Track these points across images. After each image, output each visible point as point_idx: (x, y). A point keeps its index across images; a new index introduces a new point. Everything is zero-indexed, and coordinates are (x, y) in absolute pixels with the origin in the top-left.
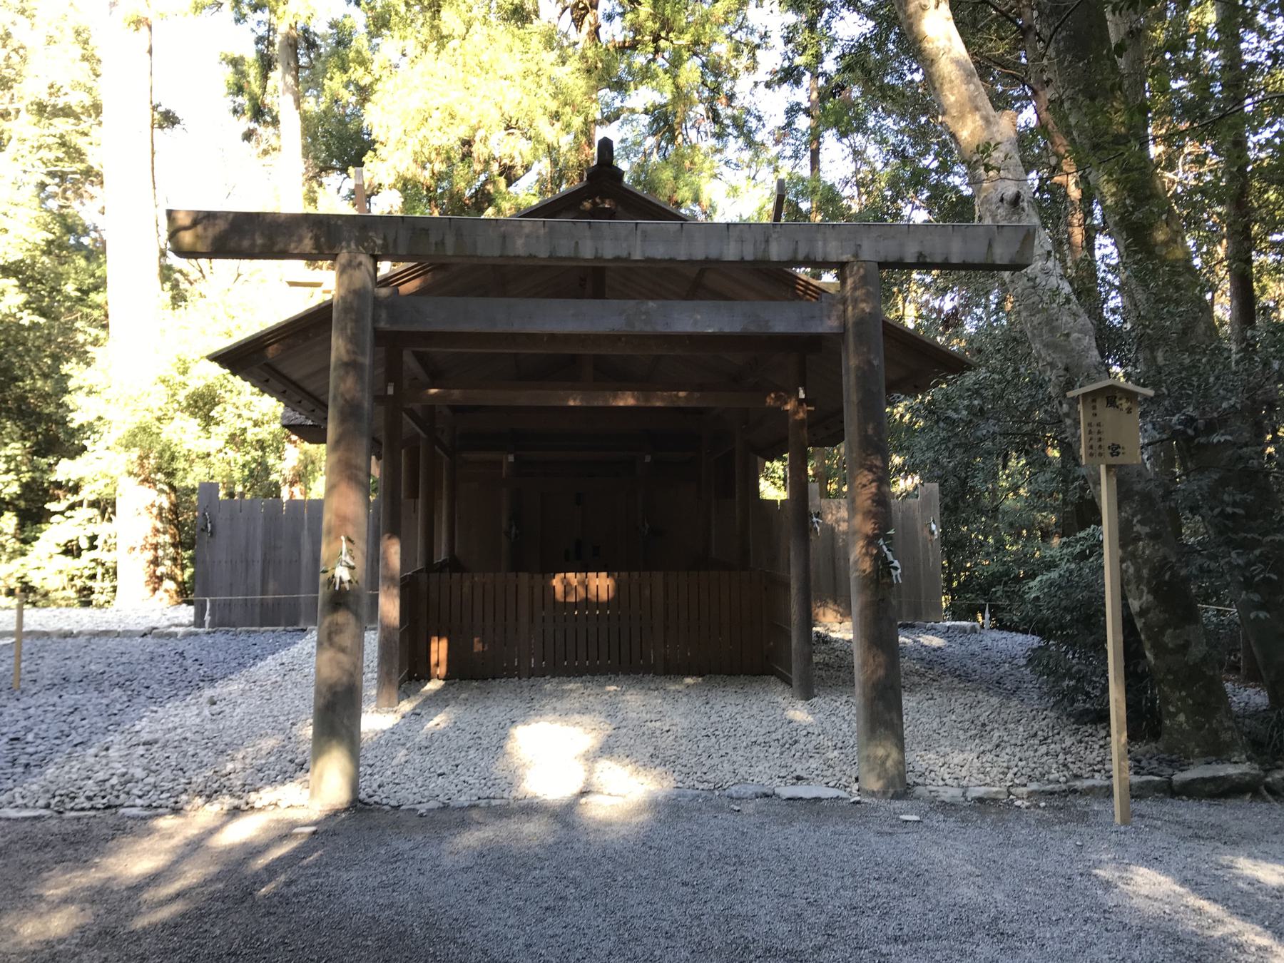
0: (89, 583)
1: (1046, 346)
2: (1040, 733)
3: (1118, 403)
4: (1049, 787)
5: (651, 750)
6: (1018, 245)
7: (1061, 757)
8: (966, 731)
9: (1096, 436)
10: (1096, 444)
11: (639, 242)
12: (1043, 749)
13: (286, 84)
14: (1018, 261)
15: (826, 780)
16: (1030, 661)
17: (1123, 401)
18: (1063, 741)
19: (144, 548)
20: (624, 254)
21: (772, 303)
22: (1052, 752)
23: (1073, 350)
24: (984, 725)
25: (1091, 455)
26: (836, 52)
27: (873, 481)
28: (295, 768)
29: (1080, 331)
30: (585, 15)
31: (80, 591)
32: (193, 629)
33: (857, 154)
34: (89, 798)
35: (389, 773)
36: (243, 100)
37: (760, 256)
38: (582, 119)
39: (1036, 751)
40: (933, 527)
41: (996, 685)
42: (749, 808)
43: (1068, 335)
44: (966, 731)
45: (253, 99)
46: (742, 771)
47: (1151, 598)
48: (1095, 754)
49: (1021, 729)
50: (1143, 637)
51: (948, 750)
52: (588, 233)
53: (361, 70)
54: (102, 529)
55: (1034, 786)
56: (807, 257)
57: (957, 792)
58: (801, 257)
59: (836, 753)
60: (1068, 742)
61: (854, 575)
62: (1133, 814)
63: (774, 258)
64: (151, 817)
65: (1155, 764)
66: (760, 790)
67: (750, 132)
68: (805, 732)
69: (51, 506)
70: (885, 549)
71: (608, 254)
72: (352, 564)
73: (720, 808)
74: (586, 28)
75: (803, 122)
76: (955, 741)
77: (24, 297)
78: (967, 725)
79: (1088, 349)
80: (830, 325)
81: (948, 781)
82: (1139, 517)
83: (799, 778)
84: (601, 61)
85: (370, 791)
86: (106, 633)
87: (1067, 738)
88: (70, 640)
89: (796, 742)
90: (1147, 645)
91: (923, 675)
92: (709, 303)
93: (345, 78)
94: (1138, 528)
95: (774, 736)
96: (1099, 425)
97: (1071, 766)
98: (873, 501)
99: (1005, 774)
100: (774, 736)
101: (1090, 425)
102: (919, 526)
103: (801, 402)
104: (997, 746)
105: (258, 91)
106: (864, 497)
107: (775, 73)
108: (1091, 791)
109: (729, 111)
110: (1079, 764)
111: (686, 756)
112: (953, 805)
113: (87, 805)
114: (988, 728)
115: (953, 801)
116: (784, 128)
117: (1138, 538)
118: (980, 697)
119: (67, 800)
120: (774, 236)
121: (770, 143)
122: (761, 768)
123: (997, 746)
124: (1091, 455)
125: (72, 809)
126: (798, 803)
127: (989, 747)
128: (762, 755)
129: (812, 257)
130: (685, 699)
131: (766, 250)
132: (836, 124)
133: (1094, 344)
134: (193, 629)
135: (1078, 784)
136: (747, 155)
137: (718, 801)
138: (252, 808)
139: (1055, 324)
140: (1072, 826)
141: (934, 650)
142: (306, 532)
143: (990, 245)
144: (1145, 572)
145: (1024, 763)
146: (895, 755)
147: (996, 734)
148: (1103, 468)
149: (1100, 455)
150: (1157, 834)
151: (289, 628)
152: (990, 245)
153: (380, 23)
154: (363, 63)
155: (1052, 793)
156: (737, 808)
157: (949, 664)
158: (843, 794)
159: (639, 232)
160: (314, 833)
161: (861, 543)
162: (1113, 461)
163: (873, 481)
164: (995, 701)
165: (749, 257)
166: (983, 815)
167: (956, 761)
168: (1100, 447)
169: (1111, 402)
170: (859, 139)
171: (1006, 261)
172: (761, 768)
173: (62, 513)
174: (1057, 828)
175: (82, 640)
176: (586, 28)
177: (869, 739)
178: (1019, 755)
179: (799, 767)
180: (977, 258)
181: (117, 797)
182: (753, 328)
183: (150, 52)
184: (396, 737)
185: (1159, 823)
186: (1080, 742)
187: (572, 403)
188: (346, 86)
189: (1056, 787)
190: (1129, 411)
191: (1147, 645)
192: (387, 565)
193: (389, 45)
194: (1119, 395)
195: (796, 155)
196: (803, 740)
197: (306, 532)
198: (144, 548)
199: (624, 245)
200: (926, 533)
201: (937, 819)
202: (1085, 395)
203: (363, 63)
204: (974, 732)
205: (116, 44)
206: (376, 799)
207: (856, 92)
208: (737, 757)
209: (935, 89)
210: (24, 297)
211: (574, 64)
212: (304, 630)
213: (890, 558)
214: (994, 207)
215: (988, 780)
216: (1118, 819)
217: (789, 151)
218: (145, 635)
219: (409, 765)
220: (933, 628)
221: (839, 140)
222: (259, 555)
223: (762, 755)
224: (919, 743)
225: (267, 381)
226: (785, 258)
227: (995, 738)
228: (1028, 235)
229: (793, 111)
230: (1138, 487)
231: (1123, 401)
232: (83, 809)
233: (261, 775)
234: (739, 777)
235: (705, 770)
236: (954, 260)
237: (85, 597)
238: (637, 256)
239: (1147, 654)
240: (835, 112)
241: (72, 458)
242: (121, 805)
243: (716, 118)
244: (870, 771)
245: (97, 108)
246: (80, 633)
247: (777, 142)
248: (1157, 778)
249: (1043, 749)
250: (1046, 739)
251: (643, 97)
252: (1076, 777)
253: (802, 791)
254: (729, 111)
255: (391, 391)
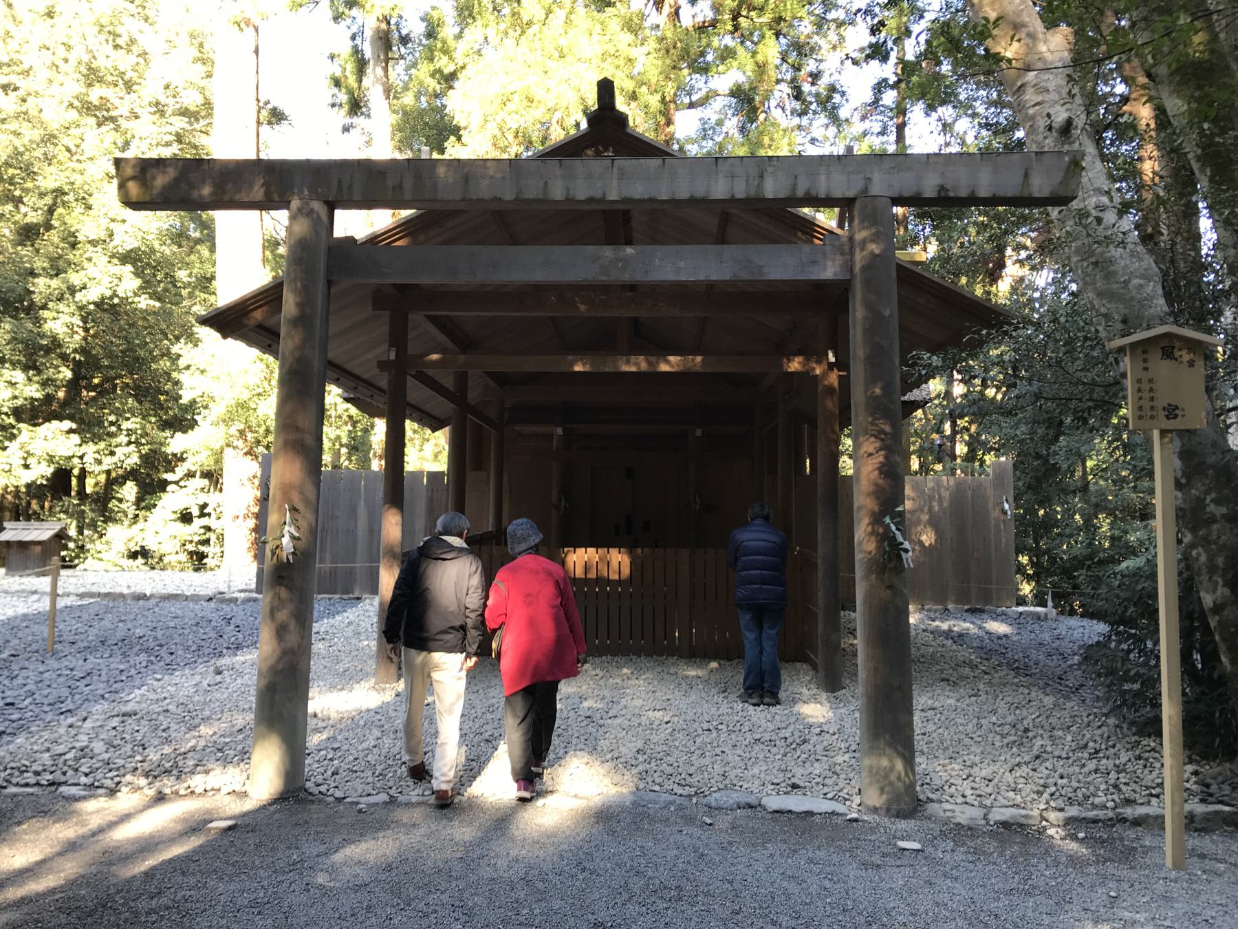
0: (202, 548)
1: (1100, 295)
2: (1091, 744)
3: (1177, 354)
4: (1091, 814)
5: (640, 744)
6: (1062, 174)
7: (1113, 775)
8: (1003, 736)
9: (1146, 395)
10: (1146, 404)
11: (615, 182)
12: (1091, 765)
14: (1062, 193)
15: (826, 790)
16: (1086, 659)
17: (1184, 353)
18: (1117, 756)
19: (246, 517)
20: (598, 195)
21: (770, 246)
22: (1102, 768)
23: (1132, 298)
24: (1026, 730)
25: (1140, 417)
26: (924, 24)
27: (881, 449)
28: (233, 753)
29: (1142, 277)
31: (191, 553)
32: (255, 595)
33: (946, 127)
34: (37, 773)
35: (351, 758)
36: (343, 97)
37: (753, 193)
38: (658, 97)
39: (1084, 765)
40: (1006, 506)
41: (1055, 682)
42: (723, 822)
43: (1126, 283)
44: (1003, 736)
45: (350, 92)
46: (732, 774)
47: (1227, 592)
48: (1154, 774)
49: (1069, 738)
50: (1217, 638)
51: (977, 759)
52: (559, 172)
53: (445, 59)
54: (213, 499)
55: (1073, 811)
56: (807, 193)
57: (977, 813)
58: (800, 193)
59: (846, 757)
60: (1124, 757)
61: (858, 557)
62: (1193, 853)
63: (769, 194)
64: (85, 798)
65: (1227, 789)
66: (743, 798)
67: (834, 108)
68: (818, 730)
69: (169, 476)
70: (893, 527)
71: (581, 194)
72: (296, 534)
73: (690, 820)
74: (666, 9)
75: (889, 97)
76: (989, 749)
77: (138, 282)
78: (1007, 729)
79: (1150, 298)
80: (830, 271)
81: (970, 799)
82: (1214, 495)
83: (795, 786)
84: (681, 41)
85: (320, 779)
86: (175, 597)
87: (1123, 753)
88: (141, 602)
89: (805, 741)
90: (1222, 648)
91: (973, 667)
92: (696, 247)
93: (432, 68)
94: (1212, 508)
95: (783, 733)
96: (1151, 381)
97: (1124, 788)
98: (881, 473)
99: (1039, 793)
100: (783, 733)
101: (1139, 381)
102: (991, 506)
103: (831, 366)
104: (1037, 757)
105: (355, 85)
106: (870, 468)
107: (862, 50)
108: (1137, 822)
109: (814, 89)
110: (1134, 786)
111: (676, 753)
112: (970, 829)
113: (32, 781)
114: (1030, 734)
115: (972, 824)
116: (874, 103)
117: (1213, 520)
118: (1033, 694)
119: (17, 773)
120: (770, 169)
121: (856, 117)
122: (756, 771)
123: (1037, 757)
124: (1140, 417)
125: (17, 785)
126: (784, 818)
127: (1027, 758)
128: (761, 757)
129: (813, 193)
130: (700, 686)
131: (760, 187)
132: (922, 96)
133: (1160, 291)
134: (255, 595)
135: (1129, 812)
136: (833, 130)
137: (693, 810)
138: (193, 792)
139: (1112, 268)
140: (1110, 868)
141: (999, 638)
142: (362, 502)
143: (1026, 175)
144: (1220, 561)
145: (1065, 781)
146: (899, 765)
147: (1038, 742)
148: (1156, 434)
149: (1152, 417)
150: (1217, 884)
151: (345, 597)
152: (1026, 175)
153: (466, 14)
154: (446, 51)
155: (1095, 821)
156: (709, 821)
157: (1009, 655)
158: (839, 808)
159: (615, 170)
160: (230, 828)
161: (866, 521)
162: (1171, 424)
163: (881, 449)
164: (1049, 701)
165: (740, 194)
166: (1003, 843)
167: (984, 773)
168: (1152, 408)
169: (1168, 353)
170: (947, 112)
171: (1045, 193)
172: (756, 771)
173: (176, 483)
174: (1092, 870)
175: (153, 602)
176: (666, 9)
177: (872, 748)
178: (1060, 771)
179: (799, 771)
181: (64, 774)
182: (744, 276)
183: (257, 52)
184: (379, 717)
185: (1222, 867)
186: (1140, 758)
187: (578, 368)
188: (433, 76)
189: (1100, 814)
190: (1191, 364)
191: (1222, 648)
193: (474, 33)
194: (1178, 344)
195: (883, 132)
196: (814, 739)
197: (362, 502)
198: (246, 517)
199: (599, 185)
201: (944, 851)
202: (1133, 346)
203: (446, 51)
204: (1012, 738)
205: (231, 50)
206: (323, 788)
207: (946, 68)
208: (731, 756)
210: (138, 282)
211: (652, 45)
212: (358, 599)
213: (900, 539)
214: (1040, 137)
215: (1019, 799)
216: (1169, 862)
217: (877, 128)
218: (211, 599)
219: (375, 751)
220: (1004, 614)
221: (927, 115)
223: (761, 757)
224: (947, 748)
225: (270, 346)
226: (782, 195)
227: (1036, 748)
228: (1076, 165)
229: (881, 86)
230: (1211, 460)
231: (1184, 353)
232: (27, 785)
233: (220, 754)
234: (727, 782)
235: (692, 770)
237: (198, 560)
238: (613, 196)
239: (1223, 659)
240: (920, 85)
241: (185, 432)
242: (65, 783)
243: (798, 95)
244: (870, 784)
245: (208, 105)
246: (152, 596)
247: (863, 118)
248: (1227, 809)
249: (1091, 765)
250: (1097, 752)
251: (725, 79)
252: (1129, 802)
253: (796, 803)
254: (814, 89)
255: (393, 356)
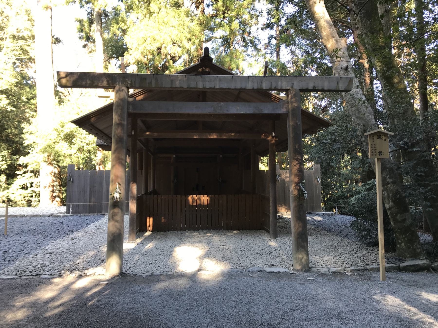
0: (31, 199)
1: (357, 118)
2: (355, 250)
3: (381, 137)
4: (358, 268)
5: (222, 255)
6: (347, 84)
7: (362, 258)
8: (329, 249)
9: (374, 149)
10: (374, 151)
11: (218, 83)
12: (356, 255)
13: (97, 29)
14: (347, 89)
15: (282, 266)
16: (351, 225)
17: (383, 137)
18: (362, 252)
19: (49, 187)
20: (213, 87)
21: (263, 103)
22: (359, 256)
23: (366, 119)
24: (336, 247)
25: (372, 155)
26: (285, 18)
27: (298, 164)
28: (101, 262)
29: (368, 113)
30: (199, 5)
31: (27, 201)
32: (66, 214)
33: (292, 52)
34: (30, 272)
35: (133, 263)
36: (83, 34)
37: (259, 87)
38: (198, 40)
39: (353, 256)
40: (318, 179)
41: (340, 233)
42: (256, 275)
43: (364, 114)
44: (329, 249)
45: (86, 34)
46: (253, 263)
47: (392, 204)
48: (373, 257)
49: (348, 248)
50: (390, 217)
51: (323, 255)
52: (200, 79)
53: (123, 24)
54: (35, 180)
55: (353, 268)
56: (275, 87)
57: (327, 270)
58: (273, 88)
59: (285, 256)
60: (364, 253)
61: (291, 196)
62: (386, 277)
63: (264, 88)
64: (51, 278)
65: (394, 260)
66: (259, 269)
67: (256, 45)
68: (274, 249)
69: (17, 172)
70: (302, 187)
71: (208, 86)
72: (120, 192)
73: (245, 275)
74: (200, 9)
75: (274, 42)
76: (326, 253)
77: (8, 101)
78: (330, 247)
79: (371, 119)
80: (283, 111)
81: (323, 266)
82: (389, 176)
83: (272, 265)
84: (205, 21)
85: (126, 269)
86: (36, 216)
87: (364, 251)
88: (24, 218)
89: (271, 253)
90: (391, 220)
91: (315, 230)
92: (242, 103)
93: (118, 27)
94: (388, 180)
95: (264, 251)
96: (375, 145)
97: (365, 261)
98: (298, 171)
99: (343, 264)
100: (264, 251)
101: (372, 145)
102: (314, 179)
103: (273, 137)
104: (340, 254)
105: (88, 31)
106: (295, 169)
107: (264, 25)
108: (372, 269)
109: (249, 38)
110: (368, 260)
111: (234, 258)
112: (325, 274)
113: (30, 274)
114: (337, 248)
115: (325, 273)
116: (267, 44)
117: (388, 183)
118: (334, 237)
119: (23, 273)
120: (264, 80)
121: (263, 49)
122: (259, 262)
123: (340, 254)
124: (372, 155)
125: (25, 276)
126: (272, 274)
127: (337, 254)
128: (260, 257)
129: (277, 88)
130: (234, 238)
131: (261, 85)
132: (285, 42)
133: (373, 117)
134: (66, 214)
135: (368, 267)
136: (255, 53)
137: (245, 273)
138: (86, 275)
139: (360, 110)
140: (366, 281)
141: (319, 221)
142: (104, 181)
143: (338, 84)
144: (391, 195)
145: (349, 260)
146: (305, 257)
147: (340, 250)
148: (376, 160)
149: (375, 155)
150: (395, 284)
151: (99, 214)
152: (338, 84)
153: (130, 8)
154: (124, 21)
155: (359, 270)
156: (251, 275)
157: (324, 226)
158: (287, 270)
159: (218, 79)
160: (107, 284)
161: (294, 185)
162: (380, 157)
163: (298, 164)
164: (339, 239)
165: (255, 87)
166: (335, 278)
167: (326, 259)
168: (375, 152)
169: (379, 137)
170: (293, 47)
171: (343, 89)
172: (259, 262)
173: (21, 175)
174: (361, 282)
175: (28, 218)
176: (200, 9)
177: (297, 252)
178: (347, 257)
179: (272, 261)
180: (333, 88)
181: (40, 271)
182: (257, 112)
183: (51, 18)
184: (135, 251)
185: (395, 280)
186: (369, 253)
187: (195, 137)
188: (118, 29)
189: (360, 268)
190: (385, 140)
191: (391, 220)
192: (132, 192)
193: (133, 15)
194: (382, 135)
195: (271, 53)
196: (274, 252)
197: (104, 181)
198: (49, 187)
199: (213, 84)
200: (316, 181)
201: (319, 279)
202: (370, 135)
203: (124, 21)
204: (332, 249)
205: (39, 15)
206: (128, 272)
207: (292, 31)
208: (251, 258)
209: (319, 30)
210: (8, 101)
211: (196, 22)
212: (104, 215)
213: (304, 190)
214: (339, 71)
215: (337, 266)
216: (381, 279)
217: (269, 52)
218: (49, 216)
219: (139, 261)
220: (318, 214)
221: (286, 48)
222: (88, 189)
223: (260, 257)
224: (314, 253)
225: (91, 130)
226: (268, 88)
227: (339, 251)
228: (351, 80)
229: (270, 38)
230: (388, 166)
231: (383, 137)
232: (28, 276)
233: (89, 264)
234: (252, 265)
235: (240, 262)
236: (326, 89)
237: (29, 203)
238: (217, 87)
239: (391, 223)
240: (285, 38)
241: (25, 156)
242: (41, 274)
243: (244, 40)
244: (297, 263)
245: (33, 37)
246: (27, 216)
247: (265, 48)
248: (395, 265)
249: (356, 255)
250: (357, 252)
251: (219, 33)
252: (367, 265)
253: (274, 269)
254: (249, 38)
255: (133, 133)
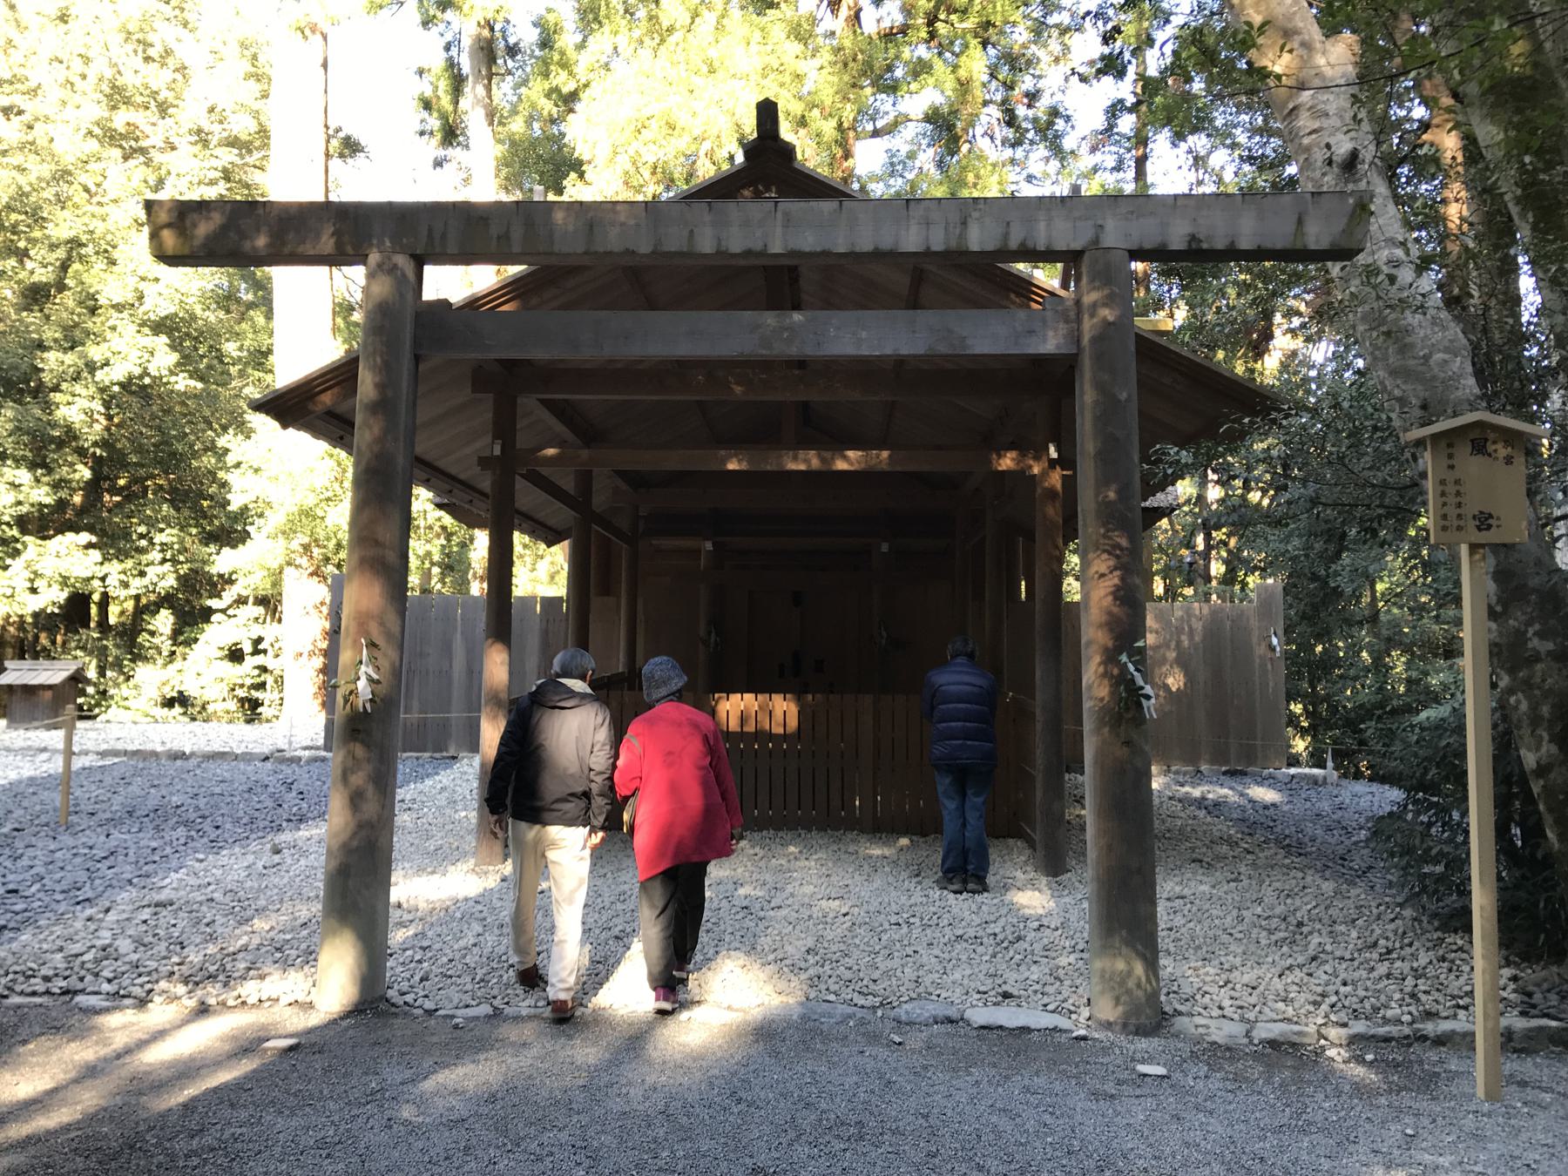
0: (255, 694)
1: (1394, 373)
2: (1382, 942)
3: (1491, 448)
4: (1382, 1031)
5: (810, 942)
6: (1345, 220)
7: (1410, 981)
8: (1270, 932)
9: (1452, 500)
10: (1452, 511)
11: (779, 230)
12: (1382, 969)
14: (1345, 244)
15: (1046, 1000)
16: (1375, 834)
17: (1499, 446)
18: (1414, 957)
19: (311, 654)
20: (758, 247)
21: (975, 311)
22: (1396, 973)
23: (1434, 378)
24: (1300, 924)
25: (1444, 528)
26: (1170, 30)
27: (1116, 568)
28: (295, 953)
29: (1446, 350)
31: (242, 701)
32: (323, 753)
33: (1199, 161)
34: (47, 979)
35: (445, 960)
36: (434, 123)
37: (953, 244)
38: (833, 123)
39: (1373, 969)
40: (1275, 641)
41: (1336, 863)
42: (916, 1040)
43: (1426, 358)
44: (1270, 932)
45: (444, 117)
46: (927, 980)
47: (1554, 749)
48: (1462, 980)
49: (1354, 934)
50: (1541, 807)
51: (1238, 961)
52: (707, 218)
53: (564, 74)
54: (269, 631)
55: (1359, 1027)
56: (1023, 244)
57: (1237, 1029)
58: (1013, 244)
59: (1072, 958)
60: (1423, 959)
61: (1087, 705)
62: (1511, 1079)
63: (974, 246)
64: (107, 1010)
65: (1554, 999)
66: (941, 1011)
67: (1056, 137)
68: (1036, 924)
69: (213, 603)
70: (1131, 668)
71: (736, 245)
72: (375, 676)
73: (874, 1038)
74: (844, 12)
75: (1127, 123)
76: (1252, 948)
77: (175, 357)
78: (1275, 922)
79: (1457, 377)
80: (1051, 343)
81: (1229, 1012)
82: (1537, 627)
83: (1006, 995)
84: (862, 52)
85: (405, 986)
86: (221, 755)
87: (1422, 953)
88: (179, 763)
89: (1019, 939)
90: (1548, 820)
91: (1233, 844)
92: (882, 313)
93: (547, 86)
94: (1535, 643)
95: (992, 928)
96: (1457, 482)
97: (1424, 998)
98: (1116, 599)
99: (1317, 1004)
100: (992, 928)
101: (1443, 482)
102: (1255, 640)
103: (1053, 464)
104: (1314, 959)
105: (450, 108)
106: (1102, 592)
107: (1092, 63)
108: (1440, 1041)
109: (1030, 113)
110: (1436, 995)
111: (856, 953)
112: (1229, 1049)
113: (41, 988)
114: (1305, 930)
115: (1230, 1043)
116: (1106, 130)
117: (1536, 658)
118: (1309, 879)
119: (22, 979)
120: (975, 215)
121: (1085, 149)
122: (957, 976)
123: (1314, 959)
124: (1444, 528)
125: (22, 993)
126: (993, 1035)
127: (1301, 960)
128: (964, 958)
129: (1030, 245)
130: (887, 869)
131: (962, 236)
132: (1168, 122)
133: (1470, 369)
134: (323, 753)
135: (1429, 1028)
136: (1054, 164)
137: (878, 1026)
138: (244, 1003)
139: (1408, 340)
140: (1406, 1099)
141: (1266, 807)
142: (459, 636)
143: (1300, 222)
144: (1545, 710)
145: (1349, 988)
146: (1139, 969)
147: (1315, 939)
148: (1464, 550)
149: (1459, 528)
150: (1542, 1119)
151: (437, 755)
152: (1300, 222)
153: (590, 17)
154: (565, 65)
155: (1387, 1039)
156: (897, 1039)
157: (1278, 829)
158: (1063, 1023)
159: (779, 215)
160: (291, 1048)
161: (1097, 659)
162: (1483, 537)
163: (1116, 568)
164: (1328, 887)
165: (937, 246)
166: (1270, 1067)
167: (1246, 979)
168: (1459, 516)
169: (1479, 447)
170: (1199, 142)
171: (1324, 244)
172: (957, 976)
173: (224, 611)
174: (1383, 1101)
175: (193, 762)
176: (844, 12)
177: (1104, 947)
178: (1343, 975)
179: (1011, 976)
181: (82, 979)
182: (943, 349)
183: (325, 65)
184: (480, 907)
185: (1548, 1097)
186: (1443, 959)
187: (732, 466)
188: (548, 96)
189: (1393, 1030)
190: (1509, 460)
191: (1548, 820)
193: (601, 42)
194: (1492, 436)
195: (1118, 168)
196: (1031, 935)
197: (459, 636)
198: (311, 654)
199: (758, 234)
201: (1195, 1077)
202: (1435, 438)
203: (565, 65)
204: (1282, 935)
205: (292, 63)
206: (409, 998)
207: (1198, 86)
208: (926, 957)
210: (175, 357)
211: (826, 56)
212: (454, 758)
213: (1140, 682)
214: (1318, 174)
215: (1290, 1012)
216: (1480, 1092)
217: (1111, 162)
218: (267, 758)
219: (475, 950)
220: (1271, 777)
221: (1174, 145)
223: (964, 958)
224: (1199, 947)
225: (342, 438)
226: (990, 247)
227: (1312, 947)
228: (1362, 209)
229: (1115, 109)
230: (1534, 582)
231: (1499, 446)
232: (34, 994)
233: (278, 955)
234: (921, 989)
235: (876, 975)
237: (251, 708)
238: (776, 248)
239: (1549, 834)
240: (1166, 108)
241: (234, 547)
242: (82, 991)
243: (1011, 120)
244: (1102, 993)
245: (263, 132)
246: (193, 754)
247: (1094, 150)
248: (1554, 1024)
249: (1382, 969)
250: (1389, 952)
251: (919, 101)
252: (1430, 1015)
253: (1008, 1016)
254: (1030, 113)
255: (497, 451)
